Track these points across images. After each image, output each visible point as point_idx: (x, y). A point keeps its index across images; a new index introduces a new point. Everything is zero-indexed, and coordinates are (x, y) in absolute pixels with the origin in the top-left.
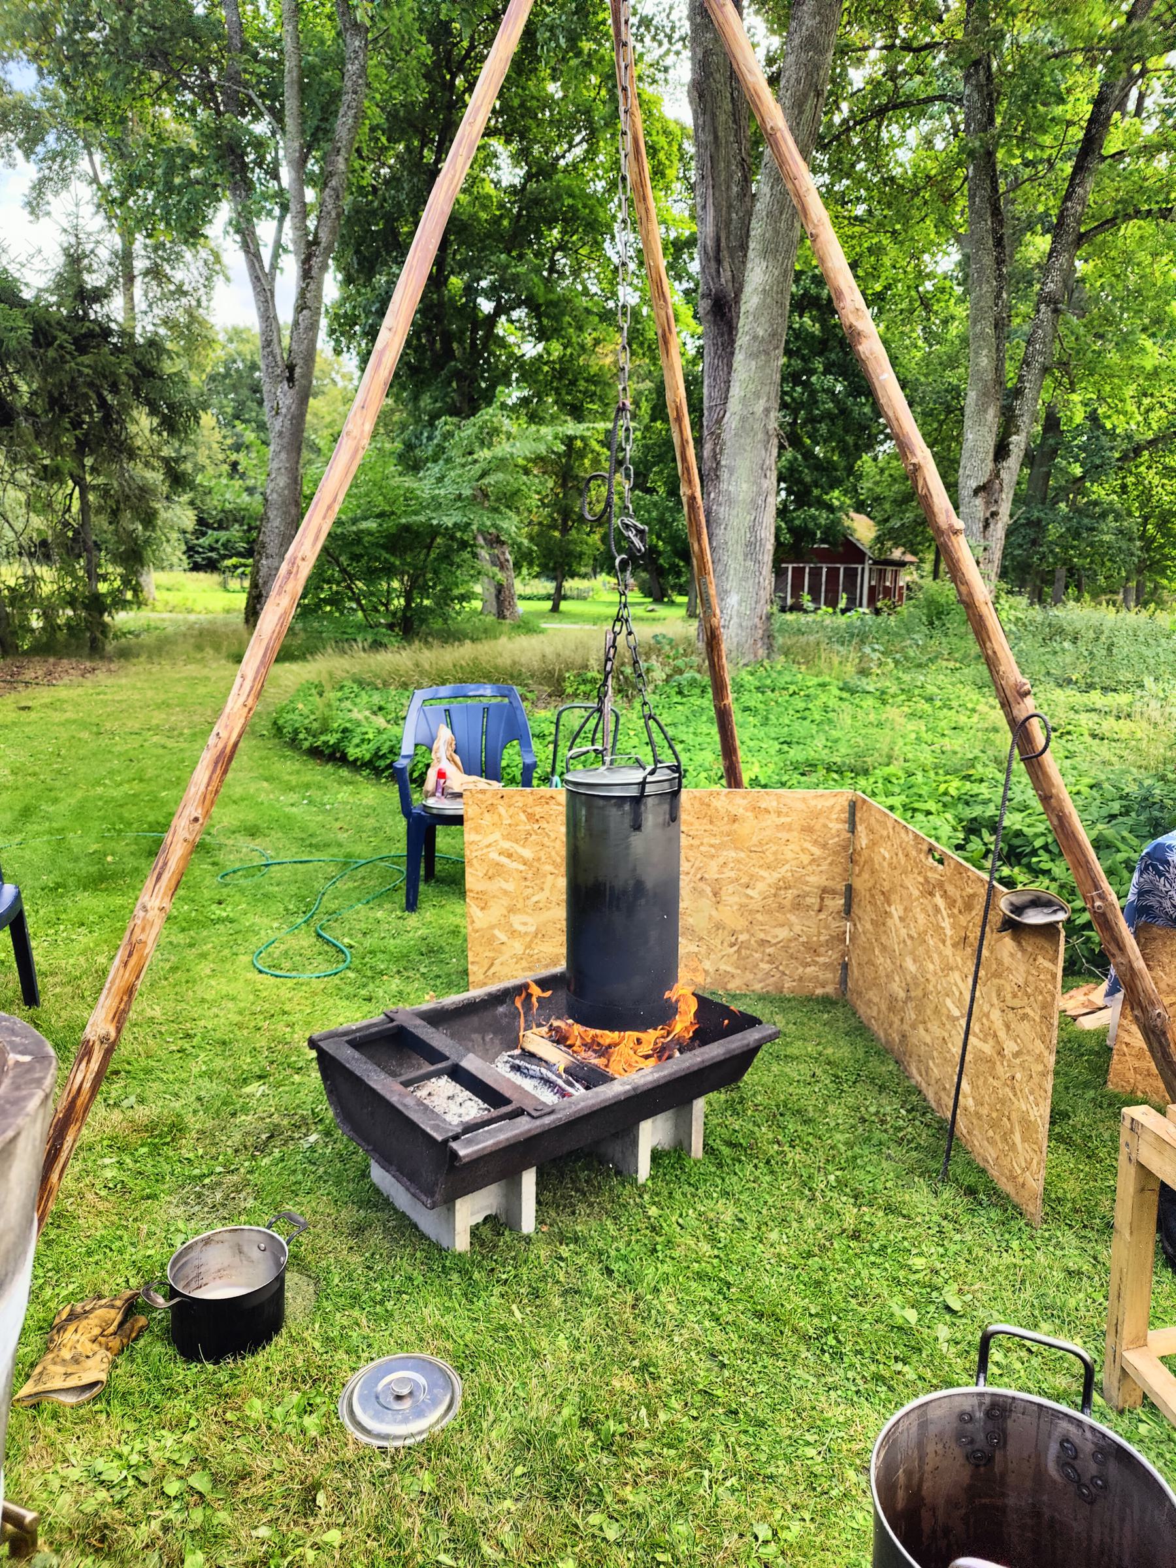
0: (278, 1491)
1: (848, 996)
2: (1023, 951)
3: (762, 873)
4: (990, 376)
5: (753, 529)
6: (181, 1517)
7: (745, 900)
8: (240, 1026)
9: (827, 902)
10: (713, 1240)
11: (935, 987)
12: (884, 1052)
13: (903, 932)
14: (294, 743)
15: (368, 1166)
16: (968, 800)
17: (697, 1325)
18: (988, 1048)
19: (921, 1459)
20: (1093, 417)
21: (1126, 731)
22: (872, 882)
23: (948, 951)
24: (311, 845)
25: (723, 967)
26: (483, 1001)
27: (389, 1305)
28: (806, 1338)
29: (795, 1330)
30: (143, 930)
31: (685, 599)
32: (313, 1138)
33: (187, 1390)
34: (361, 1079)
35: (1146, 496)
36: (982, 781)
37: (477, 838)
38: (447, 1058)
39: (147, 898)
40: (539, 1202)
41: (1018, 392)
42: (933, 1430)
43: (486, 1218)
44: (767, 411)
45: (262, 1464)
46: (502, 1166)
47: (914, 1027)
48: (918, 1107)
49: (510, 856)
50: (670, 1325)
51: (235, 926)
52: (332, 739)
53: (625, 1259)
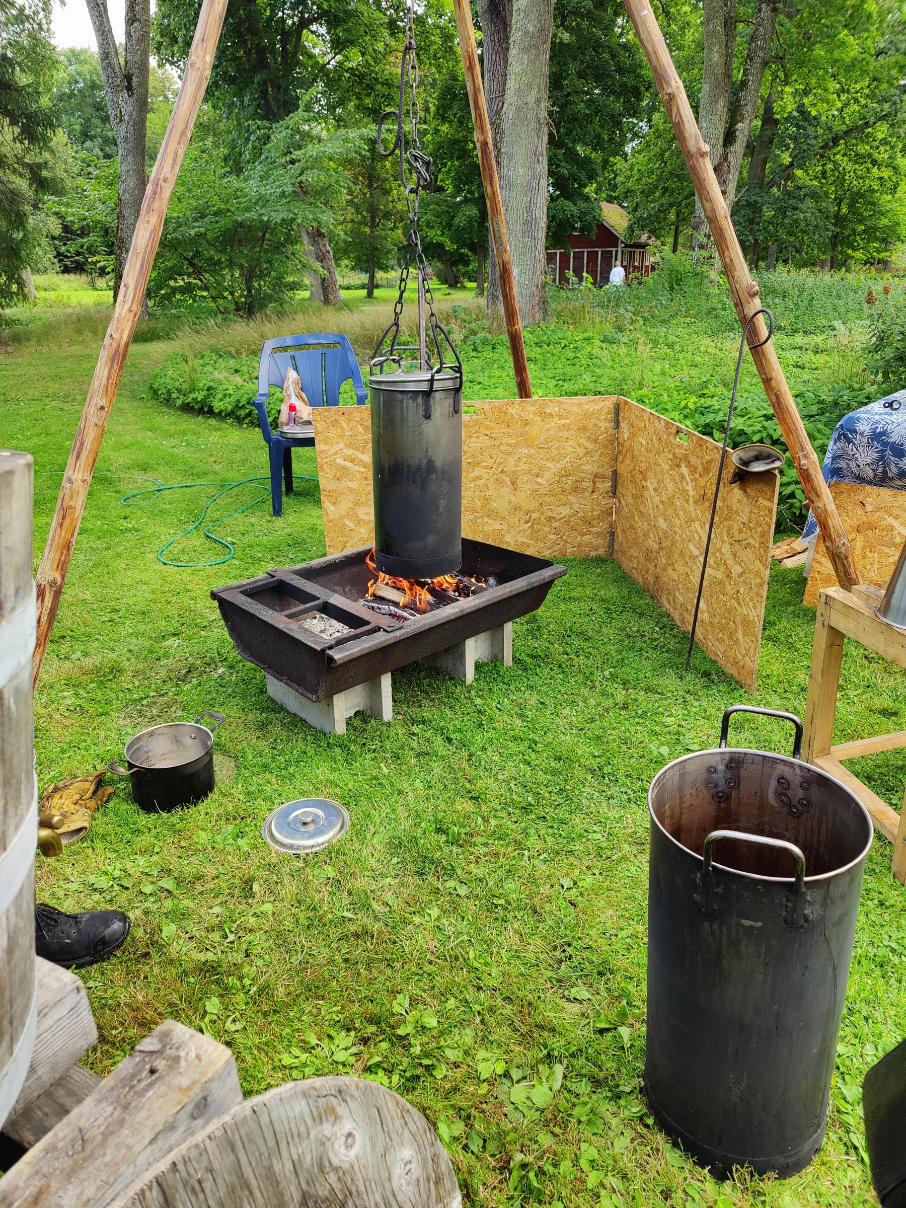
0: (224, 885)
1: (615, 556)
2: (748, 496)
3: (548, 465)
4: (720, 70)
5: (529, 209)
6: (156, 906)
7: (535, 487)
8: (154, 601)
9: (598, 485)
10: (522, 716)
11: (681, 537)
12: (642, 591)
13: (657, 499)
14: (168, 402)
16: (703, 411)
18: (720, 575)
19: (681, 799)
20: (801, 109)
21: (822, 361)
22: (632, 465)
23: (691, 507)
24: (192, 474)
25: (520, 539)
27: (291, 770)
30: (71, 498)
31: (474, 285)
32: (220, 671)
33: (150, 830)
34: (256, 623)
35: (840, 181)
36: (713, 396)
37: (326, 447)
39: (71, 472)
40: (394, 701)
41: (744, 84)
42: (689, 779)
43: (356, 713)
44: (538, 101)
45: (210, 870)
46: (365, 670)
47: (664, 569)
48: (666, 623)
49: (352, 461)
50: (496, 769)
51: (141, 534)
52: (200, 396)
53: (460, 731)
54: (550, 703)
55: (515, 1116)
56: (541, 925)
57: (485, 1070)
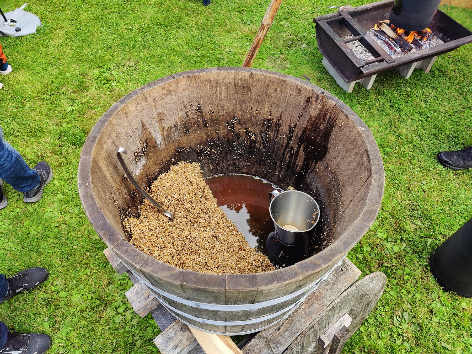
15: (322, 59)
17: (416, 126)
26: (371, 9)
28: (448, 137)
29: (445, 134)
32: (304, 45)
38: (360, 34)
53: (398, 104)
54: (440, 98)
55: (387, 252)
56: (410, 195)
57: (380, 235)
